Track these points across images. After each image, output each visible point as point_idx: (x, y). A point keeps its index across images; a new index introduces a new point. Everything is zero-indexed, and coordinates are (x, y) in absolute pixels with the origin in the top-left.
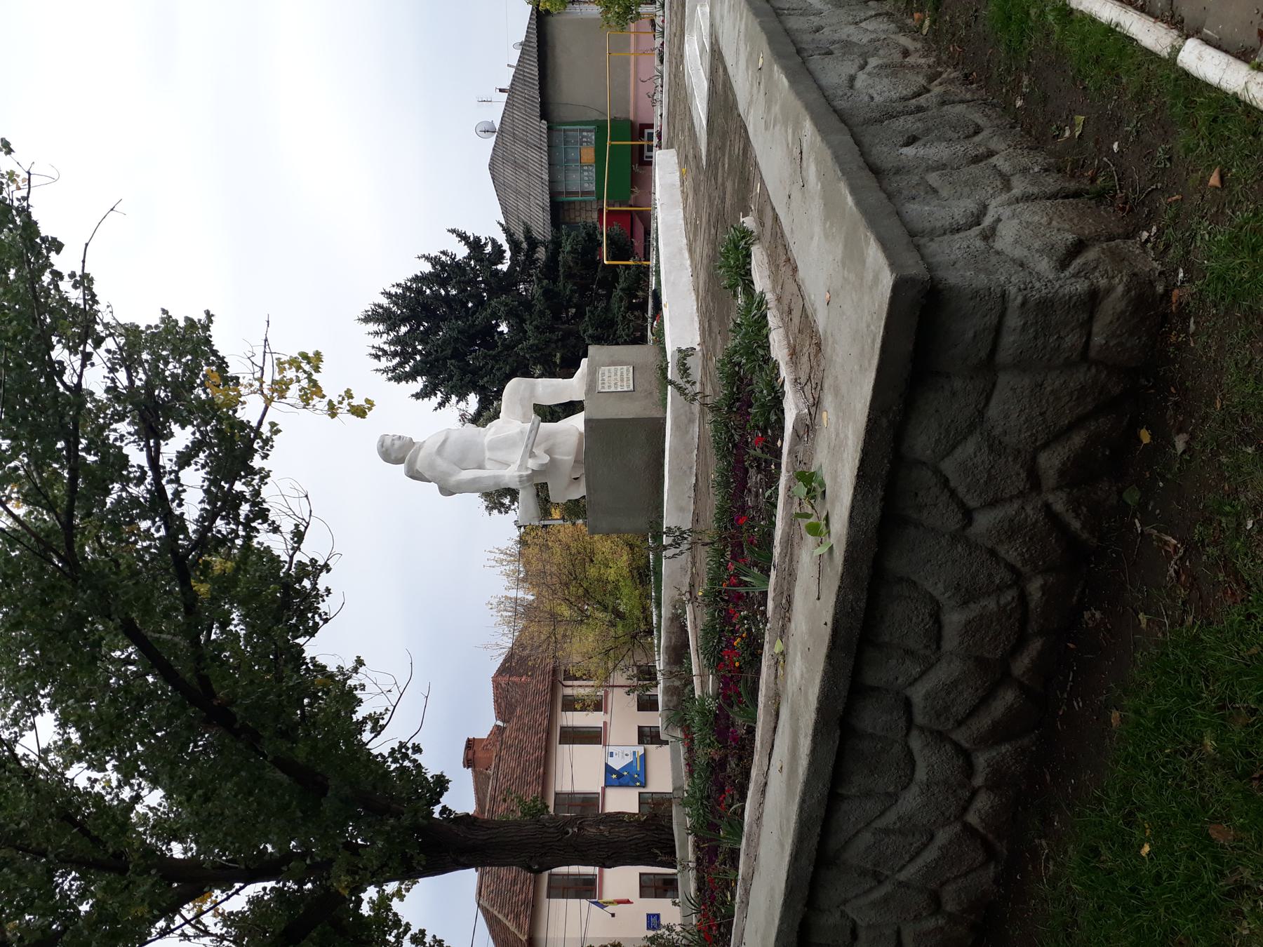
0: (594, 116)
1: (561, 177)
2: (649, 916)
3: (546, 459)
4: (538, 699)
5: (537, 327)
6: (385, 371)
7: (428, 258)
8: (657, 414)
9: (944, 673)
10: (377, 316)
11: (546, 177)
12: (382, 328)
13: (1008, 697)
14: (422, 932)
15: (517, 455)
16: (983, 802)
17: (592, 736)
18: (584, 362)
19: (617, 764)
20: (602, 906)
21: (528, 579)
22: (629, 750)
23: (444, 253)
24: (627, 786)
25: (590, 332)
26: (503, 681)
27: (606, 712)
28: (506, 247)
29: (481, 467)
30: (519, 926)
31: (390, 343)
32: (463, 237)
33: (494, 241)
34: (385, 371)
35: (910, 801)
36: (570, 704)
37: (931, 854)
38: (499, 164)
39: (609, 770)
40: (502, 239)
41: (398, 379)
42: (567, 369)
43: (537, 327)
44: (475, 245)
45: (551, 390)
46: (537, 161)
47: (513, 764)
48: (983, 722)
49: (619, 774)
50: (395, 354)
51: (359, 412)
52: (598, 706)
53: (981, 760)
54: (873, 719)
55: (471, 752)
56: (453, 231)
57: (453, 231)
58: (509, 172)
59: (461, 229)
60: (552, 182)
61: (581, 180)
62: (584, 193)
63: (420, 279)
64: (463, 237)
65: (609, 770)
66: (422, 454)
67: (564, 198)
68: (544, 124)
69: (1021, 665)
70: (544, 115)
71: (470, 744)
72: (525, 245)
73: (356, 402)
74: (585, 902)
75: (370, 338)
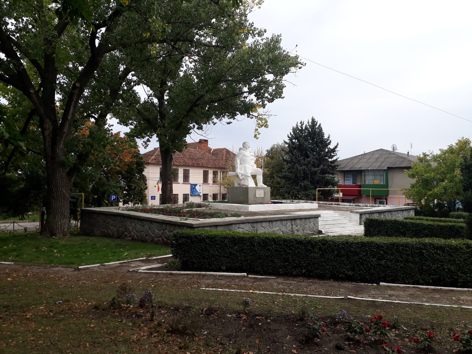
0: (390, 184)
1: (370, 173)
2: (155, 197)
3: (241, 178)
4: (217, 163)
5: (304, 169)
6: (297, 125)
7: (329, 137)
8: (249, 202)
9: (168, 232)
10: (313, 120)
11: (369, 169)
12: (310, 124)
13: (166, 240)
14: (150, 141)
15: (242, 172)
16: (157, 239)
17: (205, 180)
18: (266, 186)
19: (197, 188)
20: (157, 183)
21: (147, 199)
22: (201, 191)
23: (330, 141)
24: (191, 191)
25: (302, 184)
26: (225, 152)
27: (183, 184)
28: (333, 159)
29: (240, 164)
30: (153, 160)
31: (306, 126)
32: (336, 147)
33: (334, 156)
34: (297, 125)
35: (157, 231)
36: (215, 174)
37: (151, 234)
38: (381, 152)
39: (196, 185)
40: (334, 158)
41: (293, 129)
42: (264, 183)
43: (304, 169)
44: (333, 150)
45: (260, 178)
46: (376, 166)
47: (198, 156)
48: (164, 238)
49: (194, 188)
50: (302, 128)
51: (255, 136)
52: (214, 182)
53: (160, 238)
54: (164, 226)
55: (203, 142)
56: (338, 144)
57: (338, 144)
58: (377, 156)
59: (338, 146)
60: (368, 171)
61: (369, 180)
62: (365, 180)
63: (323, 135)
64: (336, 147)
65: (196, 185)
66: (243, 151)
67: (363, 174)
68: (386, 168)
69: (168, 241)
70: (389, 168)
71: (206, 141)
72: (333, 165)
73: (258, 136)
74: (158, 179)
75: (307, 121)
